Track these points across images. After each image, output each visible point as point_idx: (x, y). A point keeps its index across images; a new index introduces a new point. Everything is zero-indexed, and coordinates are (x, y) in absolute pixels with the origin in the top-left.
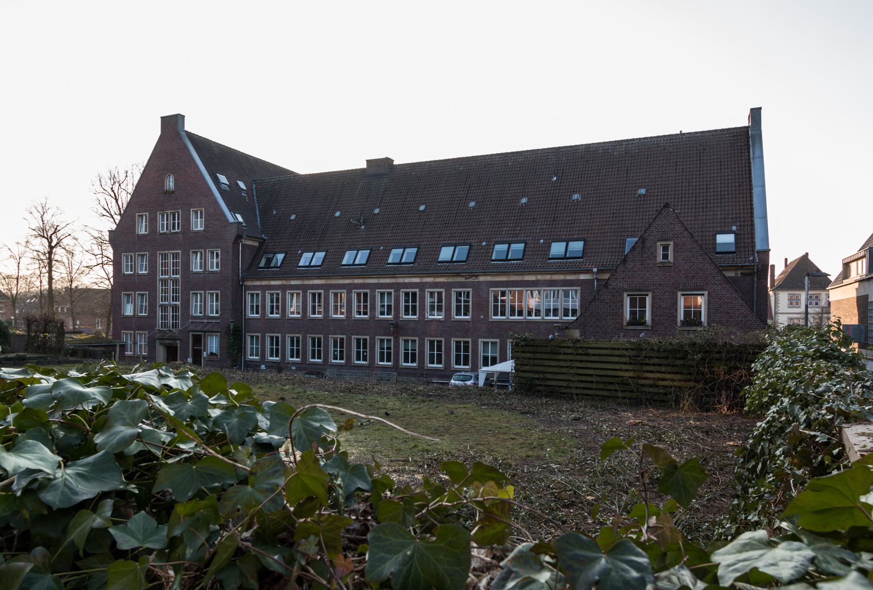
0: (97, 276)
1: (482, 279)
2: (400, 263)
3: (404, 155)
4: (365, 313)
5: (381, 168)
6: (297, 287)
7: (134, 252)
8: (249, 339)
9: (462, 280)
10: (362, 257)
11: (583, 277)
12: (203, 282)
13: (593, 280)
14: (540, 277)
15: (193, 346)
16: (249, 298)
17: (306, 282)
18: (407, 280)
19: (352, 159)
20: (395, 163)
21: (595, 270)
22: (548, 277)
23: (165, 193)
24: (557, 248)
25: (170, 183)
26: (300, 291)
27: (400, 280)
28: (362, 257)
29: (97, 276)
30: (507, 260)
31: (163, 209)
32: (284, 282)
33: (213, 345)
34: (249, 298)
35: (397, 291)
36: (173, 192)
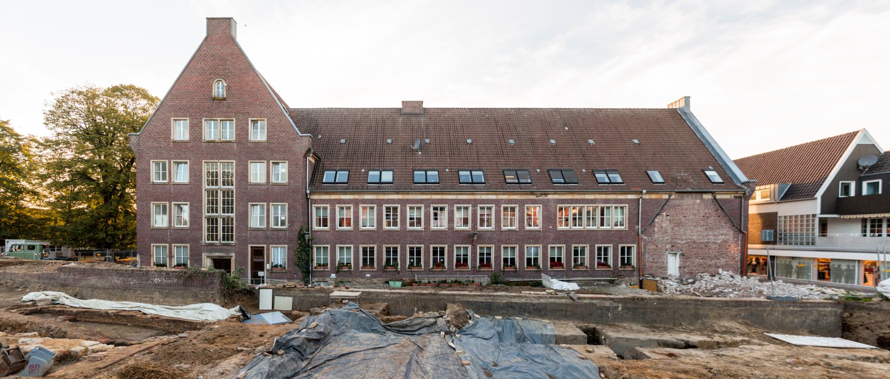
0: (286, 181)
1: (550, 197)
2: (335, 183)
3: (436, 99)
4: (395, 224)
5: (412, 112)
6: (371, 201)
7: (169, 159)
8: (315, 250)
9: (533, 197)
10: (343, 176)
11: (630, 197)
12: (268, 194)
13: (638, 200)
14: (598, 196)
15: (252, 259)
16: (314, 210)
17: (381, 197)
18: (484, 197)
19: (388, 98)
20: (425, 106)
21: (644, 191)
22: (604, 197)
23: (214, 99)
24: (373, 175)
25: (219, 89)
26: (375, 206)
27: (478, 197)
28: (343, 176)
29: (286, 181)
30: (335, 183)
31: (211, 116)
32: (357, 197)
33: (278, 255)
34: (314, 210)
35: (474, 206)
36: (224, 99)
